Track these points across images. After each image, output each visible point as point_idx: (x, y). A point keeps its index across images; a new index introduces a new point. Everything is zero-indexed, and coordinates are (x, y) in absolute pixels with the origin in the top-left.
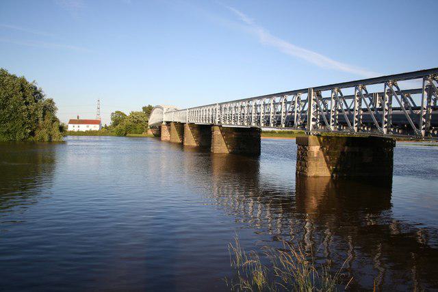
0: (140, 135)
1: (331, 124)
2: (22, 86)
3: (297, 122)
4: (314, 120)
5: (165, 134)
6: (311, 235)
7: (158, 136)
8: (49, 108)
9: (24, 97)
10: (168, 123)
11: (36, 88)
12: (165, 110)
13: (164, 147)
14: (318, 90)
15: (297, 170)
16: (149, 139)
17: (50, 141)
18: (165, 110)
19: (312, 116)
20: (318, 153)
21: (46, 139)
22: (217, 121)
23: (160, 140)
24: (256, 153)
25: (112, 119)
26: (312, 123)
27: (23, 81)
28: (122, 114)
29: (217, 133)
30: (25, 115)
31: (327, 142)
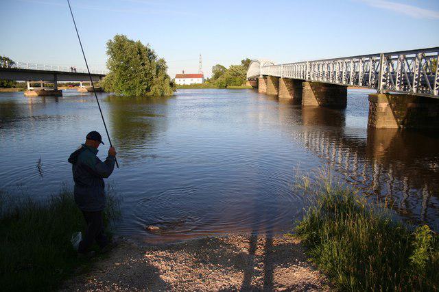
0: (240, 87)
1: (397, 85)
2: (139, 50)
3: (371, 81)
4: (384, 81)
5: (263, 87)
6: (378, 175)
7: (256, 87)
8: (161, 68)
9: (141, 59)
10: (265, 76)
11: (150, 50)
12: (262, 65)
13: (262, 99)
14: (388, 55)
15: (369, 121)
16: (248, 91)
17: (162, 95)
18: (262, 65)
19: (382, 77)
20: (386, 109)
21: (159, 93)
22: (307, 77)
23: (257, 92)
24: (343, 105)
25: (213, 72)
26: (382, 83)
27: (139, 44)
28: (222, 67)
29: (307, 87)
30: (142, 74)
31: (397, 101)
